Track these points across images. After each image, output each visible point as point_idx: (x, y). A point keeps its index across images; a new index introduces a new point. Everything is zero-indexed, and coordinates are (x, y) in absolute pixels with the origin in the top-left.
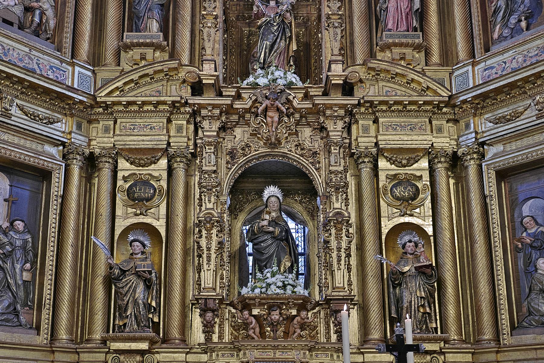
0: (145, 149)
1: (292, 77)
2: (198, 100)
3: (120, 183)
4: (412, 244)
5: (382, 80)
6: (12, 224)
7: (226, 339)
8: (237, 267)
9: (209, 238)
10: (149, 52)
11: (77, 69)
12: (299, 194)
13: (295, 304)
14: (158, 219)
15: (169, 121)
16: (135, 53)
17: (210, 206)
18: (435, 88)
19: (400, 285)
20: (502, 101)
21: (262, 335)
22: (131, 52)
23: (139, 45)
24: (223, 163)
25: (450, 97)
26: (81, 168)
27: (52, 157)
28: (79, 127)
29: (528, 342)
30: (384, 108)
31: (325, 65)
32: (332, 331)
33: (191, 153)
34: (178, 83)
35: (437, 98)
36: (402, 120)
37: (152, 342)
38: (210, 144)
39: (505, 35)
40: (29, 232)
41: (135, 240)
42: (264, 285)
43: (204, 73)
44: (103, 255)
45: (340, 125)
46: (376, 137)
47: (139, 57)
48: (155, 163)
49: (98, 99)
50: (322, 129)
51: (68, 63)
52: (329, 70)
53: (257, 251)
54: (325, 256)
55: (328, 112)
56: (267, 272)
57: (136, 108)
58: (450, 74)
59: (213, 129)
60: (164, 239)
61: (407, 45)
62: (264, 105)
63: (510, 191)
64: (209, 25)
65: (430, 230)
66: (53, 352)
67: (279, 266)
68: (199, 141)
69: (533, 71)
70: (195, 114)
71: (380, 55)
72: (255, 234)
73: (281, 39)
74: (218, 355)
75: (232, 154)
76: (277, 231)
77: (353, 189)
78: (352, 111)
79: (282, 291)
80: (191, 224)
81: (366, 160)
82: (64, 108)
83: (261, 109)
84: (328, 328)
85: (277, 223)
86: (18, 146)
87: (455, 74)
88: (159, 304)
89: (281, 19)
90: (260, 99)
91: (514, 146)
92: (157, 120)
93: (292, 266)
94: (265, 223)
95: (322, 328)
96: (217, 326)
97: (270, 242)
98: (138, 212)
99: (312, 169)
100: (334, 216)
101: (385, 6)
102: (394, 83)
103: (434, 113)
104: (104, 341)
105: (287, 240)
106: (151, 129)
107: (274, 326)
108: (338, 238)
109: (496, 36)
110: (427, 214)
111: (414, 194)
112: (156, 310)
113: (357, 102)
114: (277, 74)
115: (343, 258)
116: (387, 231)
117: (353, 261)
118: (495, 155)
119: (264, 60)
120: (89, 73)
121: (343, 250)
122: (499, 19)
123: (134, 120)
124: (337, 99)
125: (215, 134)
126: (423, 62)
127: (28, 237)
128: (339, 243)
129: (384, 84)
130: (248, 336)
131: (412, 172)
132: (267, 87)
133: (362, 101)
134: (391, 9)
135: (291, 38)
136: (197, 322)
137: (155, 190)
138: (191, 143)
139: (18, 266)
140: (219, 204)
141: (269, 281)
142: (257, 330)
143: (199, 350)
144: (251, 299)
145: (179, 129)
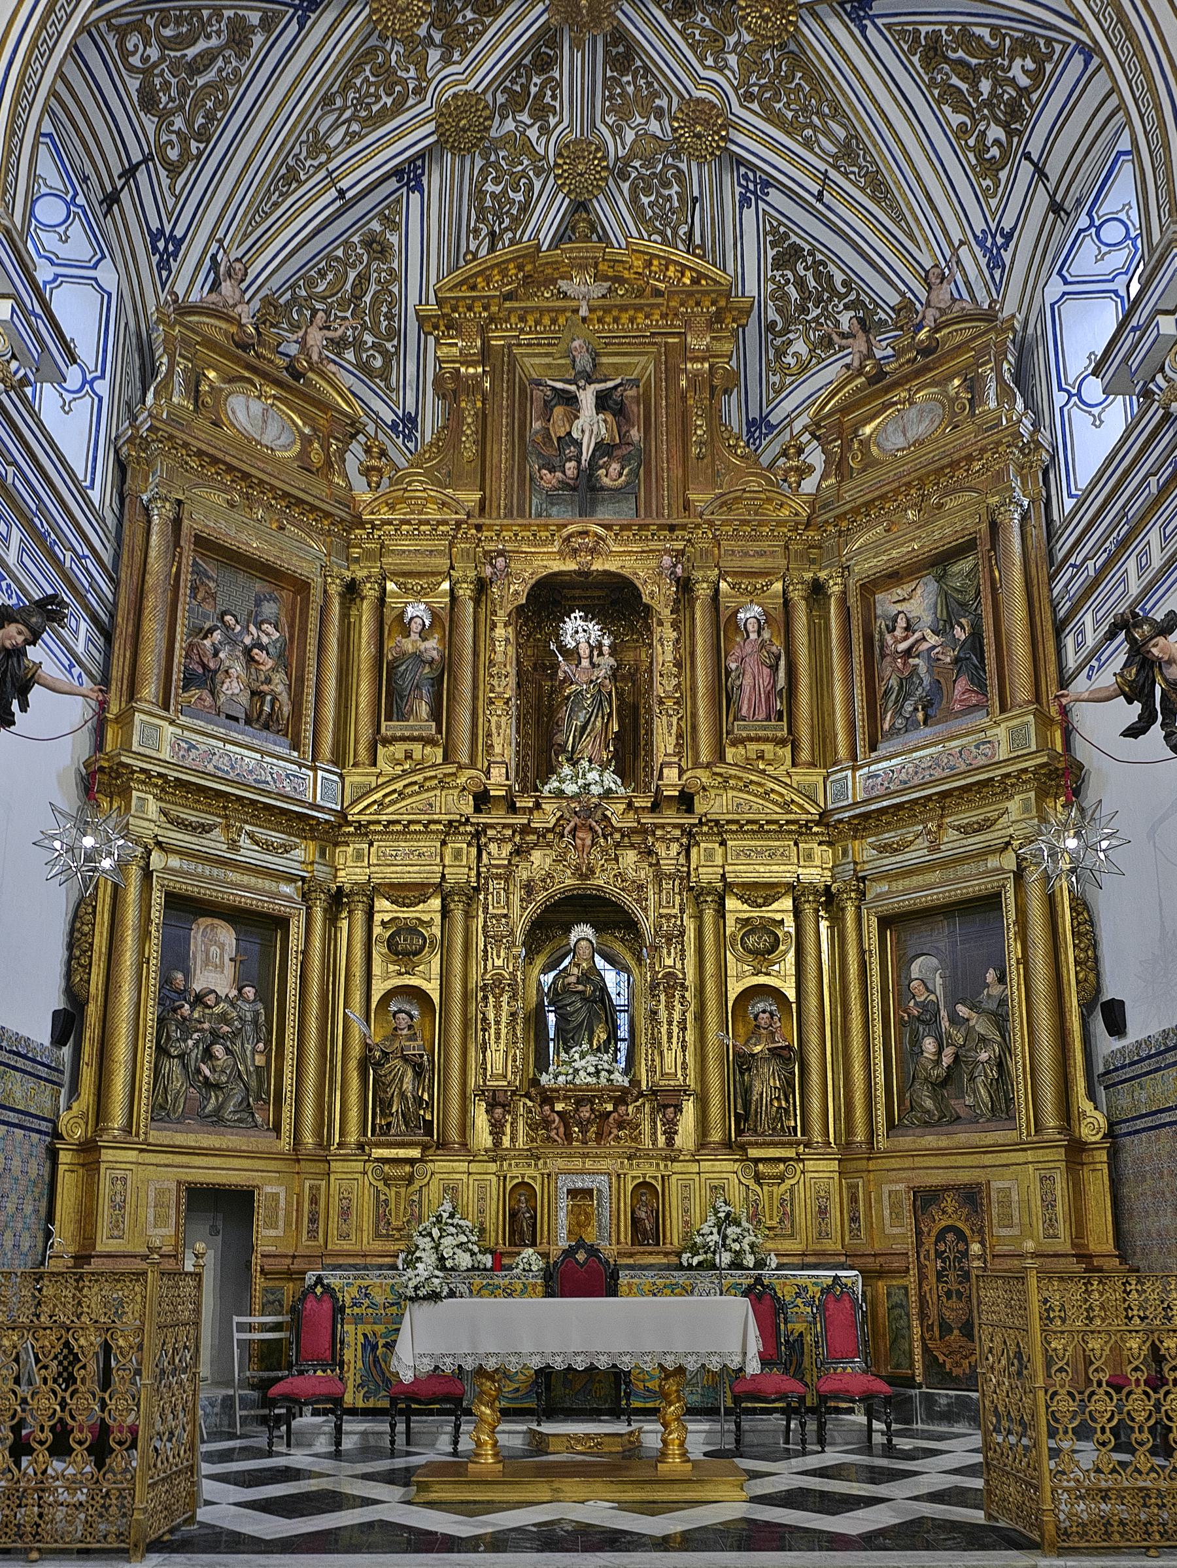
0: (412, 884)
1: (610, 780)
2: (483, 819)
3: (377, 930)
4: (767, 1015)
5: (732, 788)
6: (240, 990)
7: (521, 1142)
8: (532, 1034)
9: (498, 1007)
10: (417, 749)
11: (320, 773)
12: (620, 929)
13: (611, 1097)
14: (429, 980)
15: (444, 843)
16: (399, 749)
17: (499, 963)
18: (801, 802)
19: (749, 1069)
20: (888, 823)
21: (568, 1136)
22: (392, 748)
23: (403, 739)
24: (515, 900)
25: (820, 815)
26: (325, 910)
27: (289, 898)
28: (323, 854)
29: (906, 1147)
30: (734, 827)
31: (657, 767)
32: (659, 1132)
33: (473, 888)
34: (456, 792)
35: (804, 817)
36: (758, 843)
37: (425, 1147)
38: (498, 877)
39: (897, 726)
40: (261, 1000)
41: (400, 1011)
42: (571, 1071)
43: (492, 781)
44: (357, 1028)
45: (675, 847)
46: (723, 867)
47: (402, 756)
48: (424, 902)
49: (350, 818)
50: (650, 852)
51: (308, 767)
52: (660, 777)
53: (562, 1018)
54: (653, 1030)
55: (659, 832)
56: (575, 1052)
57: (399, 828)
58: (825, 779)
59: (504, 855)
60: (437, 1008)
61: (766, 740)
62: (572, 824)
63: (898, 938)
64: (499, 712)
65: (791, 995)
66: (298, 1161)
67: (590, 1042)
68: (482, 869)
69: (923, 794)
70: (477, 835)
71: (730, 753)
72: (559, 994)
73: (597, 716)
74: (510, 1165)
75: (529, 888)
76: (589, 989)
77: (692, 936)
78: (691, 831)
79: (594, 1080)
80: (472, 985)
81: (709, 899)
82: (304, 830)
83: (568, 829)
84: (654, 1127)
85: (588, 978)
86: (247, 888)
87: (831, 778)
88: (431, 1097)
89: (597, 688)
90: (567, 815)
91: (900, 885)
92: (427, 844)
93: (609, 1037)
94: (573, 979)
95: (646, 1127)
96: (508, 1125)
97: (579, 1005)
98: (403, 970)
99: (635, 907)
100: (664, 977)
101: (738, 683)
102: (748, 793)
103: (801, 834)
104: (361, 1146)
105: (602, 1001)
106: (419, 855)
107: (584, 1126)
108: (670, 1007)
109: (886, 726)
110: (788, 973)
111: (772, 946)
112: (430, 1105)
113: (697, 821)
114: (593, 776)
115: (675, 1035)
116: (735, 996)
117: (690, 1036)
118: (878, 895)
119: (573, 747)
120: (335, 778)
121: (675, 1023)
122: (890, 704)
123: (396, 844)
124: (670, 816)
125: (506, 862)
126: (789, 762)
127: (260, 1007)
128: (670, 1014)
129: (735, 793)
130: (549, 1137)
131: (770, 915)
132: (575, 797)
133: (704, 820)
134: (747, 689)
135: (610, 715)
136: (481, 1120)
137: (425, 939)
138: (473, 873)
139: (249, 1047)
140: (511, 958)
141: (577, 1065)
142: (562, 1130)
143: (486, 1158)
144: (552, 1090)
145: (457, 854)
